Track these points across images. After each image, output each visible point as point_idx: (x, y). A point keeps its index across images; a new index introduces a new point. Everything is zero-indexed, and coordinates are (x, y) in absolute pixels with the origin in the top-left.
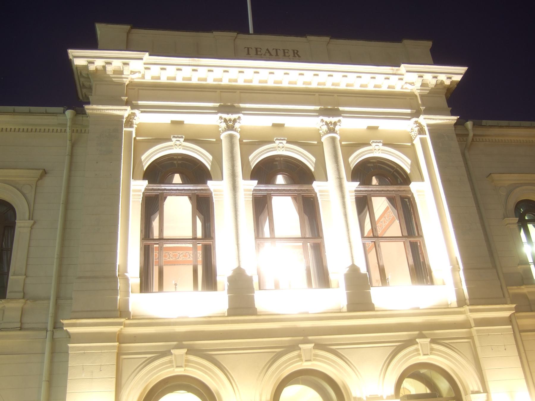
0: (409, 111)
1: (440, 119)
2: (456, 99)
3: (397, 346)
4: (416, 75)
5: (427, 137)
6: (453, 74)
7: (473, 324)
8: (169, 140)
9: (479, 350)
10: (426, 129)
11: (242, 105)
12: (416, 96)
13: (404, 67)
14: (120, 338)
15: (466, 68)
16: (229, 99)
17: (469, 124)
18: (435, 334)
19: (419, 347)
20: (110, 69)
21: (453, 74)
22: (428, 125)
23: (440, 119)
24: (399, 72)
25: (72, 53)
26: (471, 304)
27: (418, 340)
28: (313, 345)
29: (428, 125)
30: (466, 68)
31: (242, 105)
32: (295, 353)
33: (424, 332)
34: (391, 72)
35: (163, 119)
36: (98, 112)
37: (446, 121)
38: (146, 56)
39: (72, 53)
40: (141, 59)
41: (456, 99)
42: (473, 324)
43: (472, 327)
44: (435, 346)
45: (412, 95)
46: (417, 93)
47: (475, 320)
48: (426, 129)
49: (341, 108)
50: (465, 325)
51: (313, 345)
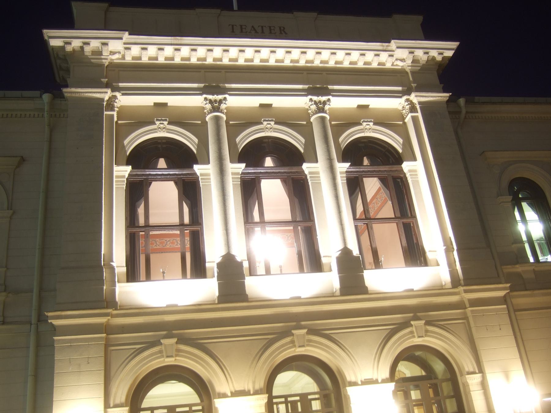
0: (400, 88)
2: (445, 75)
3: (392, 329)
5: (419, 115)
6: (443, 50)
9: (474, 330)
10: (418, 107)
12: (407, 73)
13: (393, 44)
14: (108, 329)
16: (214, 79)
17: (462, 101)
21: (443, 50)
22: (420, 103)
23: (432, 97)
24: (389, 48)
27: (412, 323)
28: (305, 331)
29: (420, 103)
31: (228, 86)
32: (288, 339)
33: (419, 314)
34: (381, 48)
36: (77, 95)
38: (126, 36)
40: (121, 39)
46: (408, 69)
47: (470, 300)
48: (418, 107)
50: (459, 305)
51: (305, 331)
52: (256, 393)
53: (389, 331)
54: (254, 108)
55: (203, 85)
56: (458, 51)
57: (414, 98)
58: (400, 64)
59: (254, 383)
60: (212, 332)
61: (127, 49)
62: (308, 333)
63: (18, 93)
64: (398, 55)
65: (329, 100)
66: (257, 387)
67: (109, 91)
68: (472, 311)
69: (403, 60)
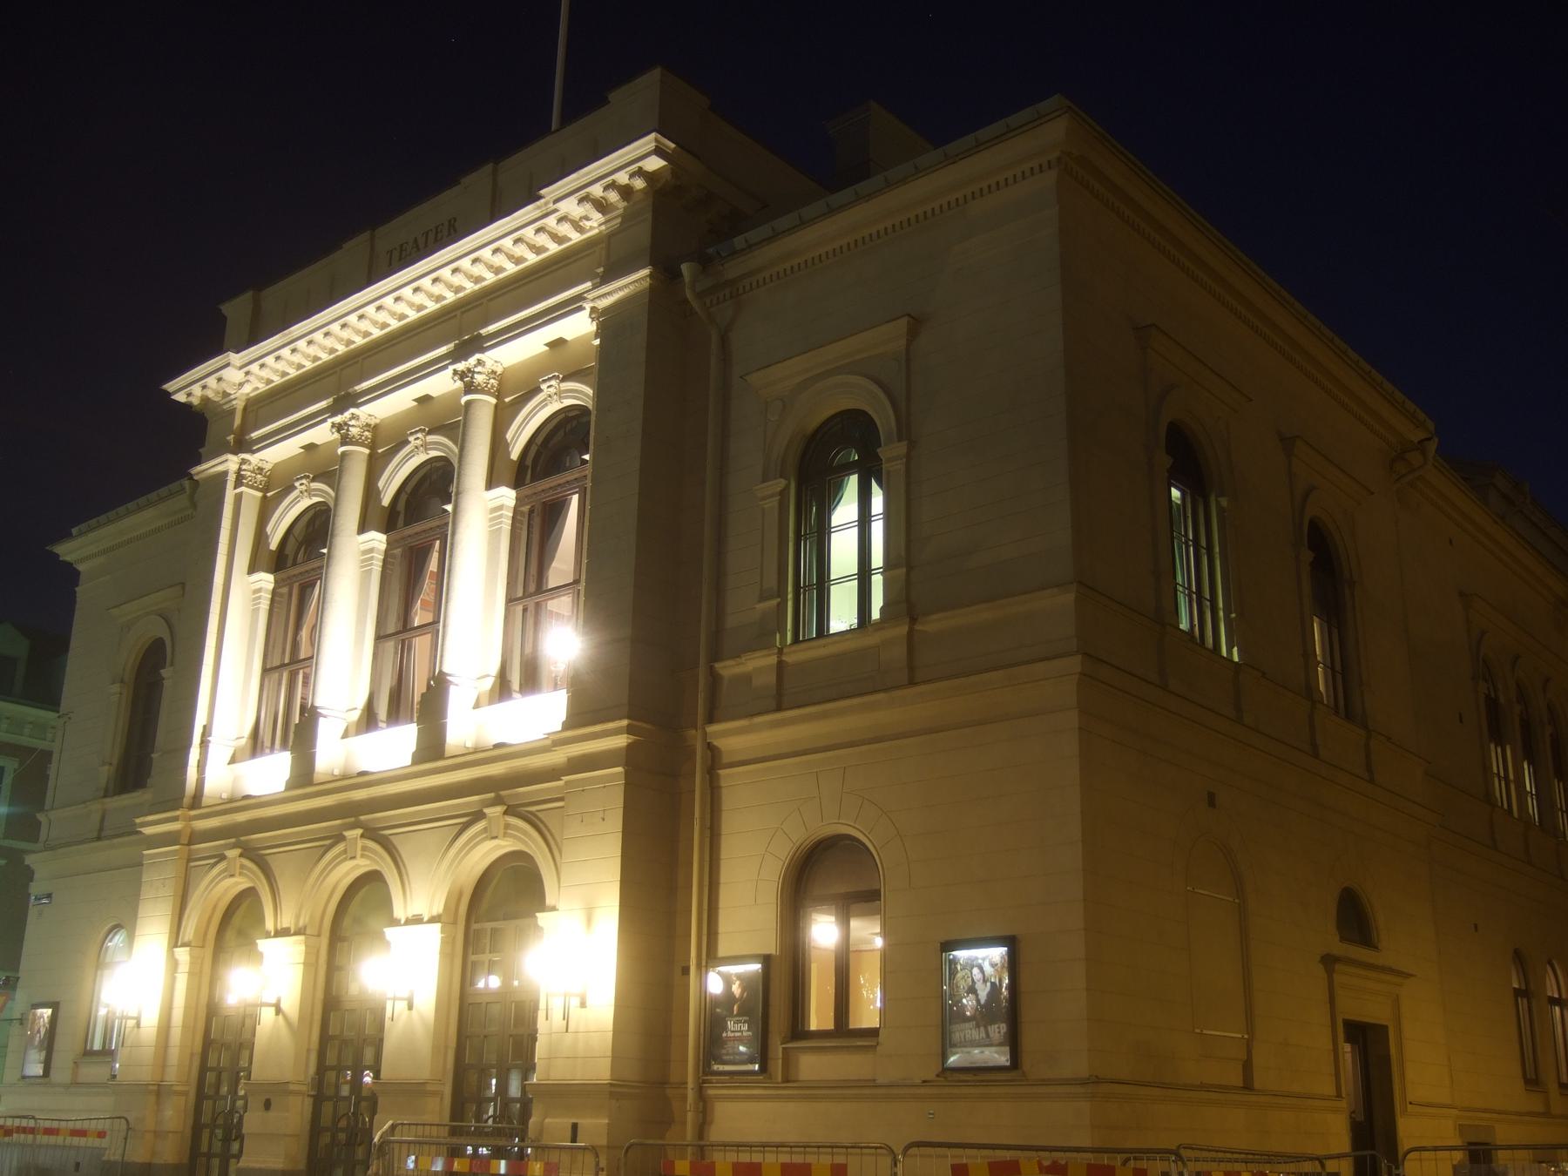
0: (323, 404)
1: (620, 289)
4: (573, 200)
8: (538, 390)
11: (359, 388)
14: (196, 837)
16: (338, 382)
18: (518, 794)
20: (210, 394)
22: (225, 473)
23: (620, 289)
25: (170, 386)
31: (359, 388)
32: (340, 847)
33: (503, 793)
34: (538, 213)
35: (399, 402)
37: (620, 294)
38: (235, 358)
39: (170, 386)
40: (228, 365)
49: (484, 332)
52: (433, 920)
54: (409, 412)
55: (331, 400)
59: (298, 917)
61: (247, 373)
63: (969, 140)
65: (480, 363)
66: (435, 913)
67: (230, 456)
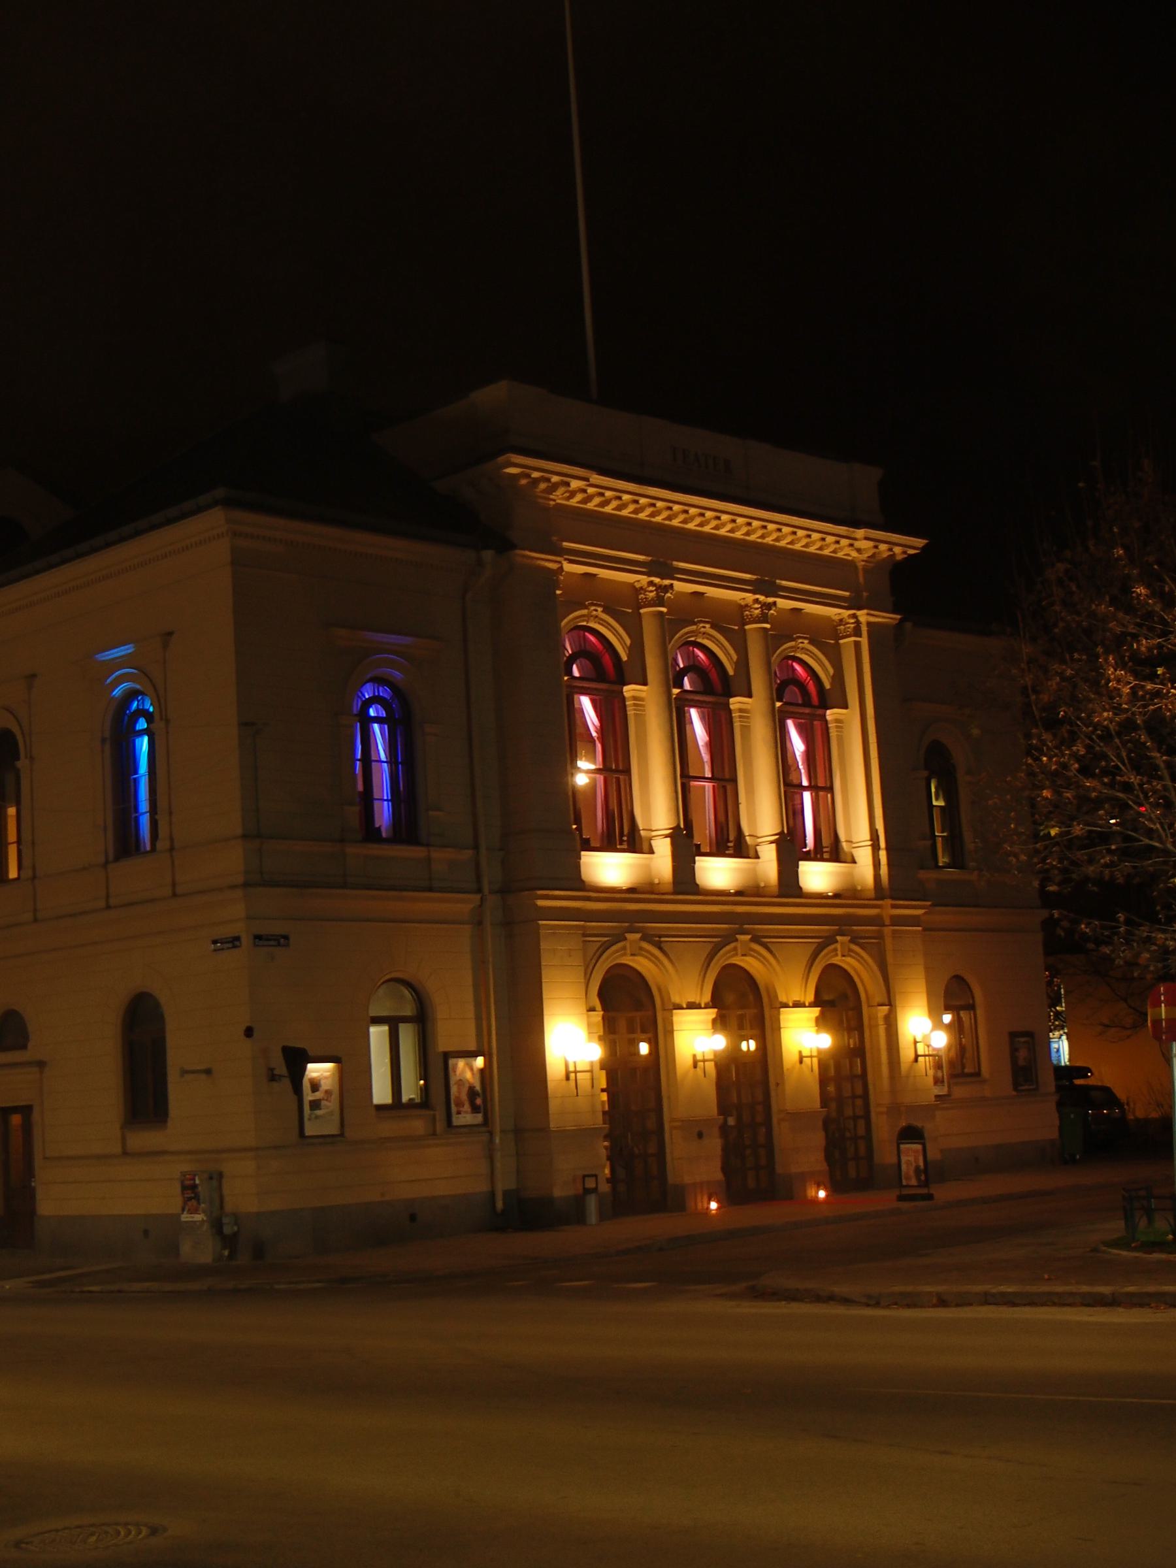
2: (899, 585)
3: (716, 944)
5: (864, 641)
6: (904, 546)
7: (887, 922)
10: (864, 629)
12: (856, 567)
13: (860, 533)
15: (925, 541)
19: (738, 945)
21: (904, 546)
22: (869, 624)
24: (853, 536)
26: (893, 898)
29: (869, 624)
30: (925, 541)
34: (844, 533)
41: (899, 585)
42: (887, 922)
43: (884, 925)
44: (645, 945)
45: (849, 565)
46: (860, 565)
47: (892, 917)
48: (864, 629)
50: (876, 921)
53: (815, 946)
56: (924, 549)
57: (863, 616)
58: (854, 554)
60: (669, 928)
62: (752, 940)
64: (858, 546)
68: (894, 932)
69: (859, 551)
